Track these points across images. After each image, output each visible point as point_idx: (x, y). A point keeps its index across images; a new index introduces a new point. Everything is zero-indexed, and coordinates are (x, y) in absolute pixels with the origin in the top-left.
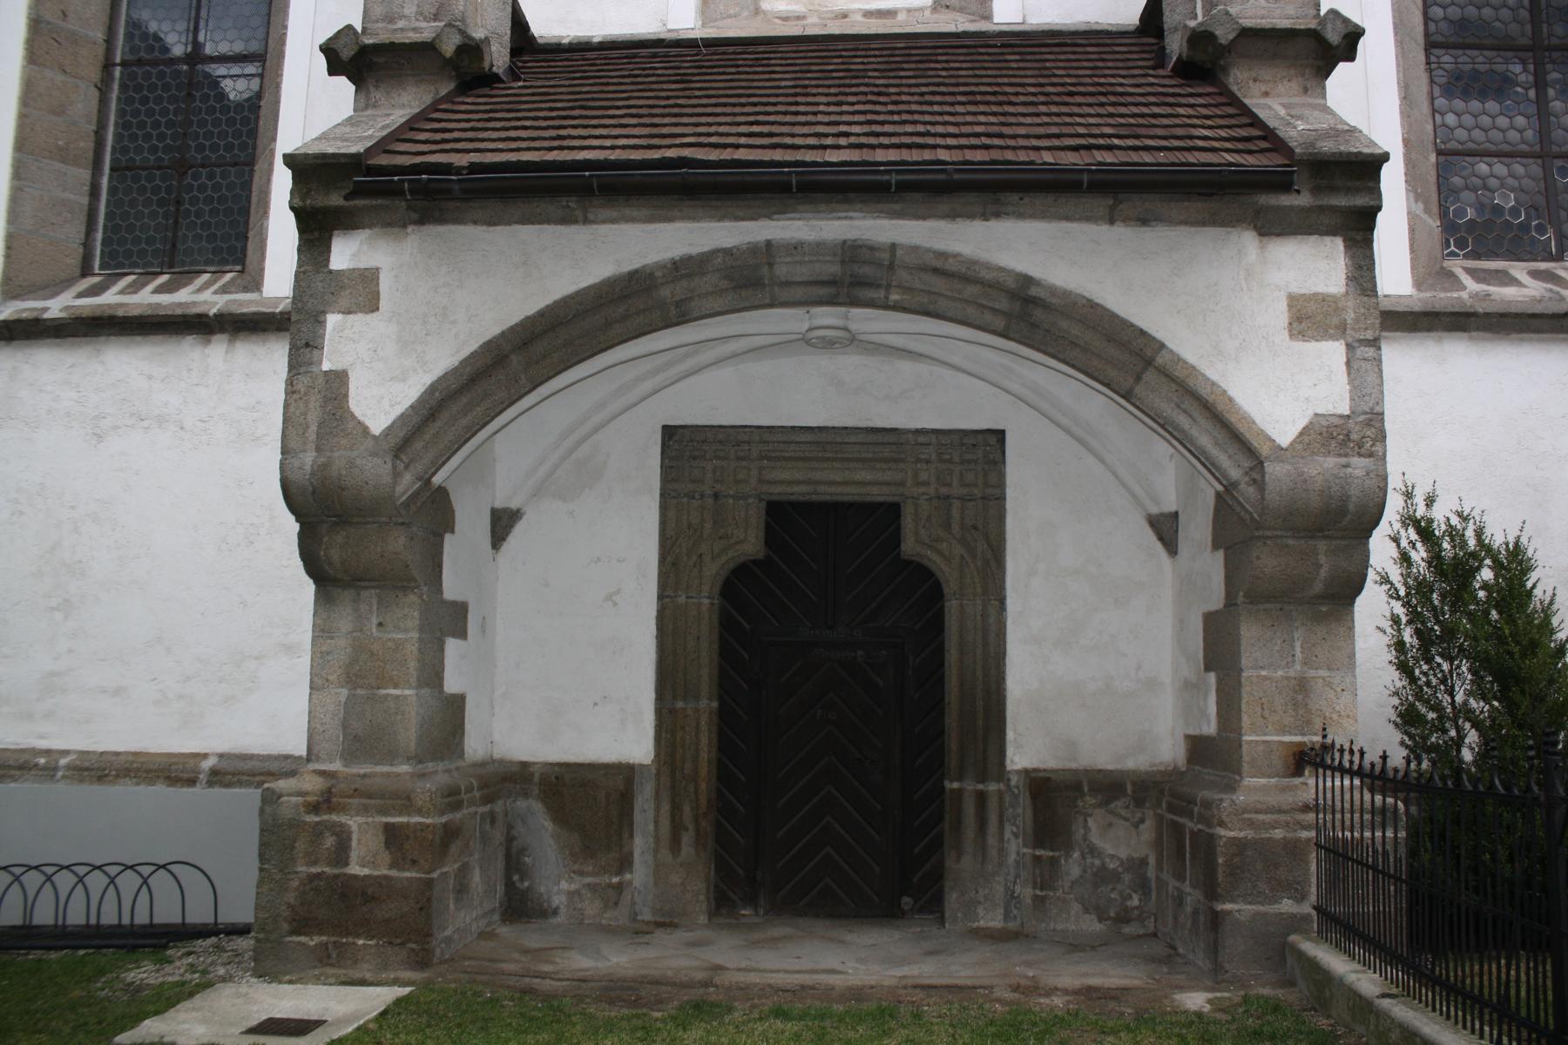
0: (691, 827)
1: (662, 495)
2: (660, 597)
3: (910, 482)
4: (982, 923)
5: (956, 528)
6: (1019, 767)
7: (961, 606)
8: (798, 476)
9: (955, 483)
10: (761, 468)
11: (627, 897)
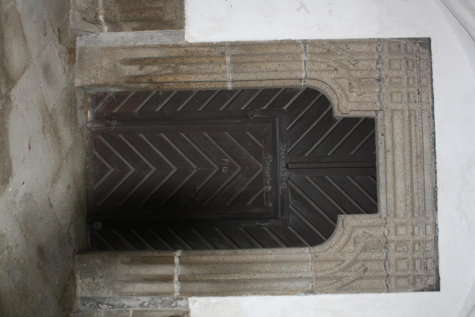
0: (142, 72)
1: (379, 40)
2: (305, 42)
3: (398, 221)
4: (79, 281)
5: (364, 256)
6: (191, 307)
7: (308, 261)
8: (398, 139)
9: (397, 254)
10: (402, 111)
11: (95, 28)
